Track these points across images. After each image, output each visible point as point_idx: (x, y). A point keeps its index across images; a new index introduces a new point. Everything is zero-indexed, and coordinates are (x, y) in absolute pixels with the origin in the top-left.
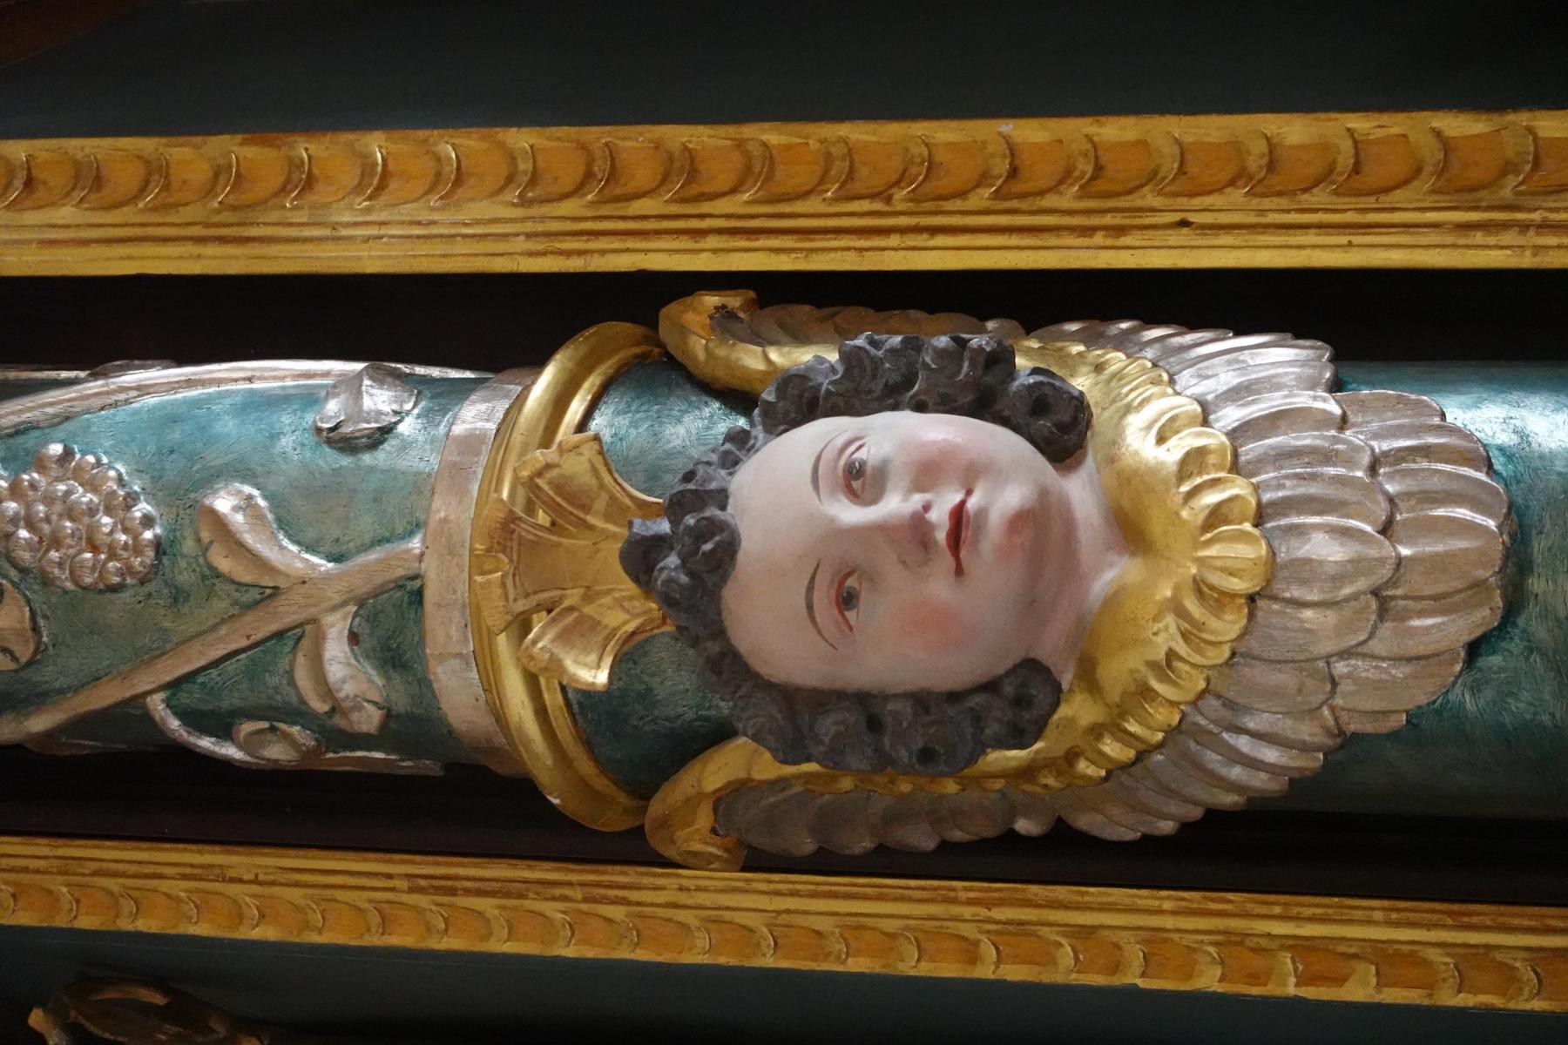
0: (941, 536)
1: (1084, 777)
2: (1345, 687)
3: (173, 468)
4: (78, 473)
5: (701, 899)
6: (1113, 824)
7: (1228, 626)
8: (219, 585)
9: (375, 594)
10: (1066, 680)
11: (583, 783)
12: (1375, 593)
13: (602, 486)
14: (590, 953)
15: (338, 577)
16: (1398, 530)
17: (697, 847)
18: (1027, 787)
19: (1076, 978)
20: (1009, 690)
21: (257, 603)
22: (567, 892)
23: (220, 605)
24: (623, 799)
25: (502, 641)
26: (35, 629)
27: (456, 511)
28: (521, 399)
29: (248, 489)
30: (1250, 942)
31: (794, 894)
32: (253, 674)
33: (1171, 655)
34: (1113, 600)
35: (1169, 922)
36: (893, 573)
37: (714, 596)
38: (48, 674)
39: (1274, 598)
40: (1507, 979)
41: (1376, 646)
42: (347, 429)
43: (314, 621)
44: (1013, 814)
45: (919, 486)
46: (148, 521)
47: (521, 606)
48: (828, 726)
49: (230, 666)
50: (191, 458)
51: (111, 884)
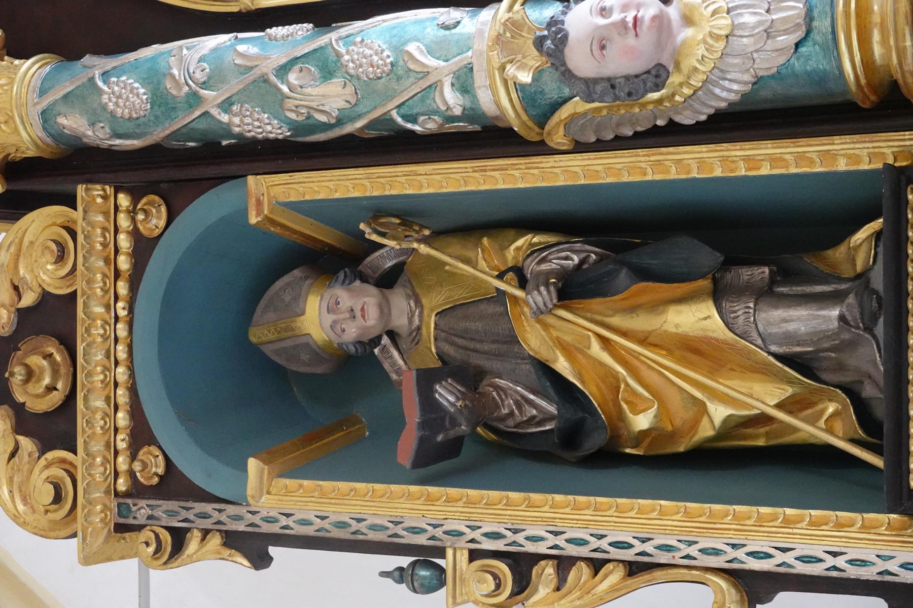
0: (631, 25)
1: (677, 101)
2: (758, 61)
3: (395, 41)
4: (366, 45)
5: (562, 164)
6: (686, 119)
7: (721, 45)
8: (411, 74)
9: (458, 71)
10: (671, 69)
11: (524, 123)
12: (765, 31)
13: (526, 23)
14: (528, 186)
15: (448, 66)
16: (772, 11)
17: (560, 140)
18: (660, 107)
19: (677, 177)
20: (653, 72)
21: (422, 78)
22: (520, 166)
23: (411, 80)
24: (537, 129)
25: (496, 72)
26: (356, 93)
27: (481, 45)
28: (498, 9)
29: (418, 44)
30: (730, 159)
31: (589, 159)
32: (422, 100)
33: (703, 56)
34: (684, 42)
35: (705, 155)
36: (616, 37)
37: (562, 52)
38: (361, 109)
39: (734, 36)
40: (812, 162)
41: (767, 47)
42: (447, 23)
43: (440, 81)
44: (656, 118)
45: (623, 11)
46: (388, 57)
47: (504, 60)
48: (599, 88)
49: (415, 98)
50: (400, 37)
51: (382, 180)
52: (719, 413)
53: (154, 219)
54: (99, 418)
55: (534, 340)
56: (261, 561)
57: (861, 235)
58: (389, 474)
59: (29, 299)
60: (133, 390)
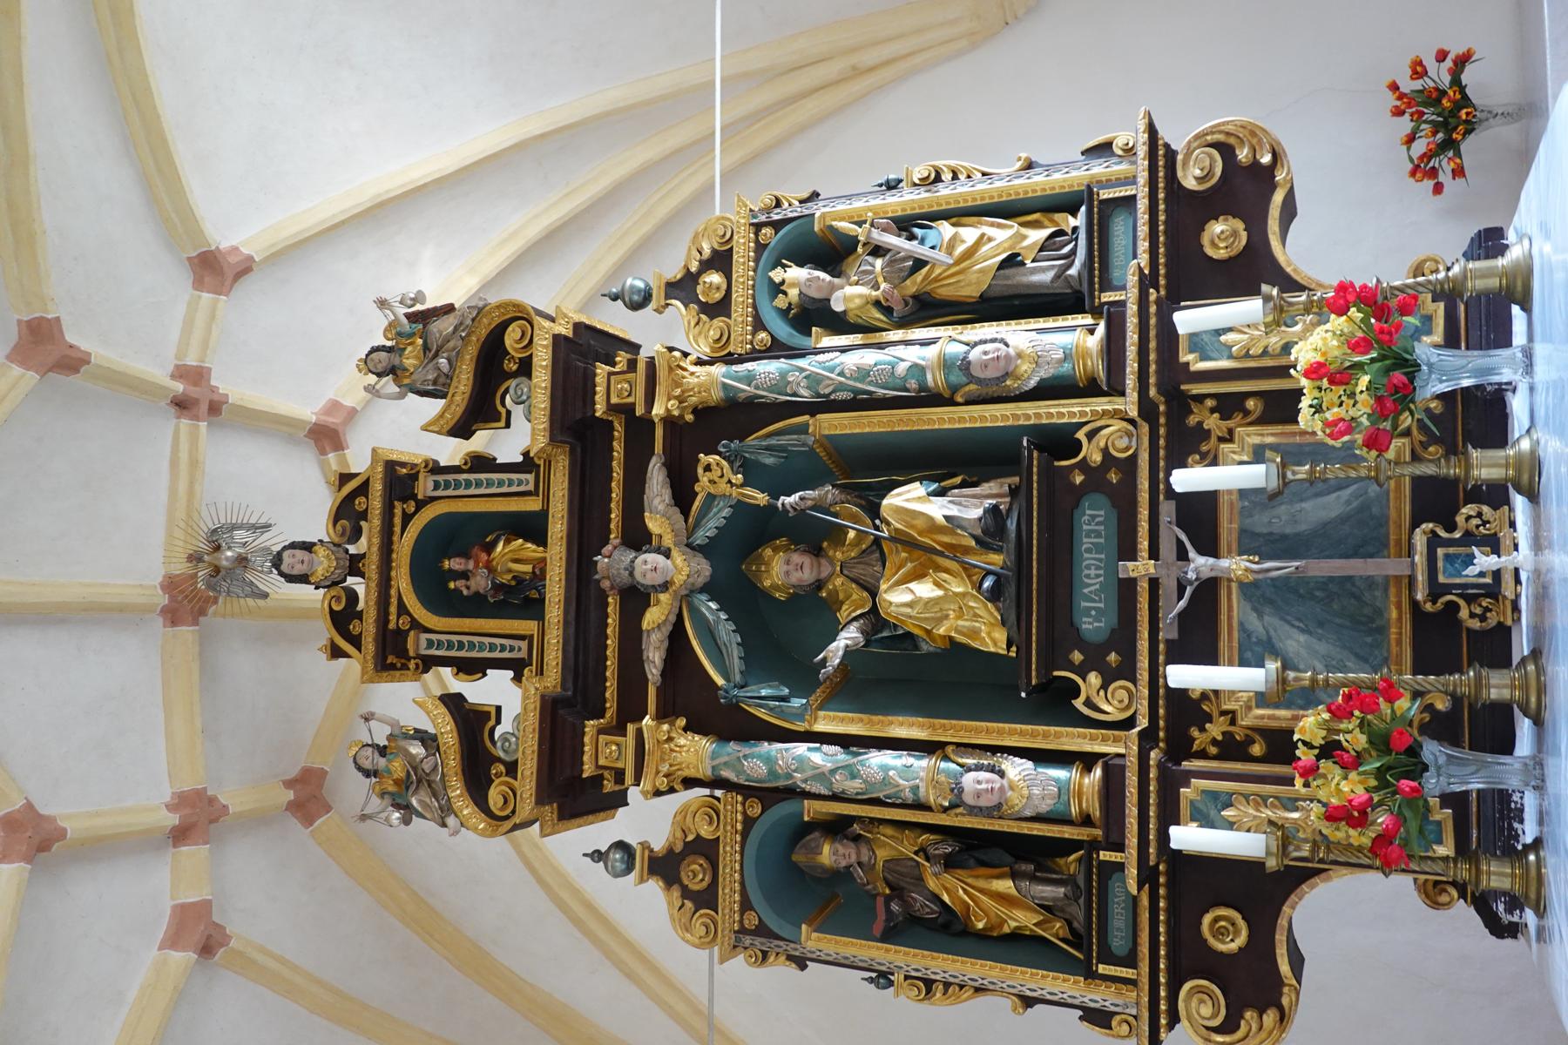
52: (1013, 924)
53: (756, 810)
54: (729, 895)
55: (932, 884)
56: (803, 967)
57: (1072, 857)
58: (869, 937)
59: (690, 838)
60: (742, 884)
